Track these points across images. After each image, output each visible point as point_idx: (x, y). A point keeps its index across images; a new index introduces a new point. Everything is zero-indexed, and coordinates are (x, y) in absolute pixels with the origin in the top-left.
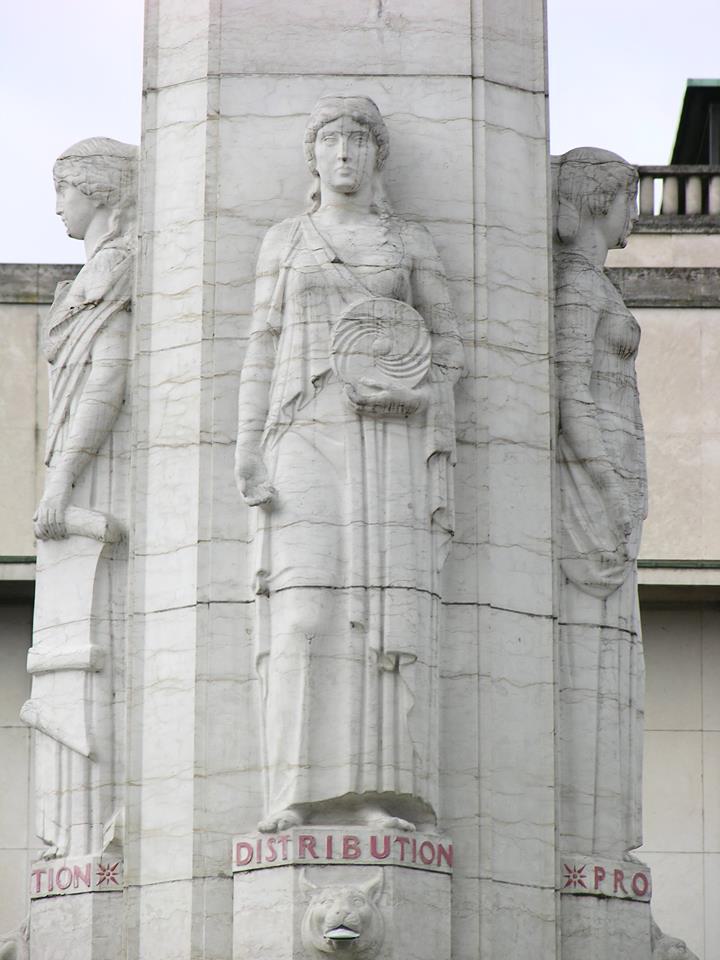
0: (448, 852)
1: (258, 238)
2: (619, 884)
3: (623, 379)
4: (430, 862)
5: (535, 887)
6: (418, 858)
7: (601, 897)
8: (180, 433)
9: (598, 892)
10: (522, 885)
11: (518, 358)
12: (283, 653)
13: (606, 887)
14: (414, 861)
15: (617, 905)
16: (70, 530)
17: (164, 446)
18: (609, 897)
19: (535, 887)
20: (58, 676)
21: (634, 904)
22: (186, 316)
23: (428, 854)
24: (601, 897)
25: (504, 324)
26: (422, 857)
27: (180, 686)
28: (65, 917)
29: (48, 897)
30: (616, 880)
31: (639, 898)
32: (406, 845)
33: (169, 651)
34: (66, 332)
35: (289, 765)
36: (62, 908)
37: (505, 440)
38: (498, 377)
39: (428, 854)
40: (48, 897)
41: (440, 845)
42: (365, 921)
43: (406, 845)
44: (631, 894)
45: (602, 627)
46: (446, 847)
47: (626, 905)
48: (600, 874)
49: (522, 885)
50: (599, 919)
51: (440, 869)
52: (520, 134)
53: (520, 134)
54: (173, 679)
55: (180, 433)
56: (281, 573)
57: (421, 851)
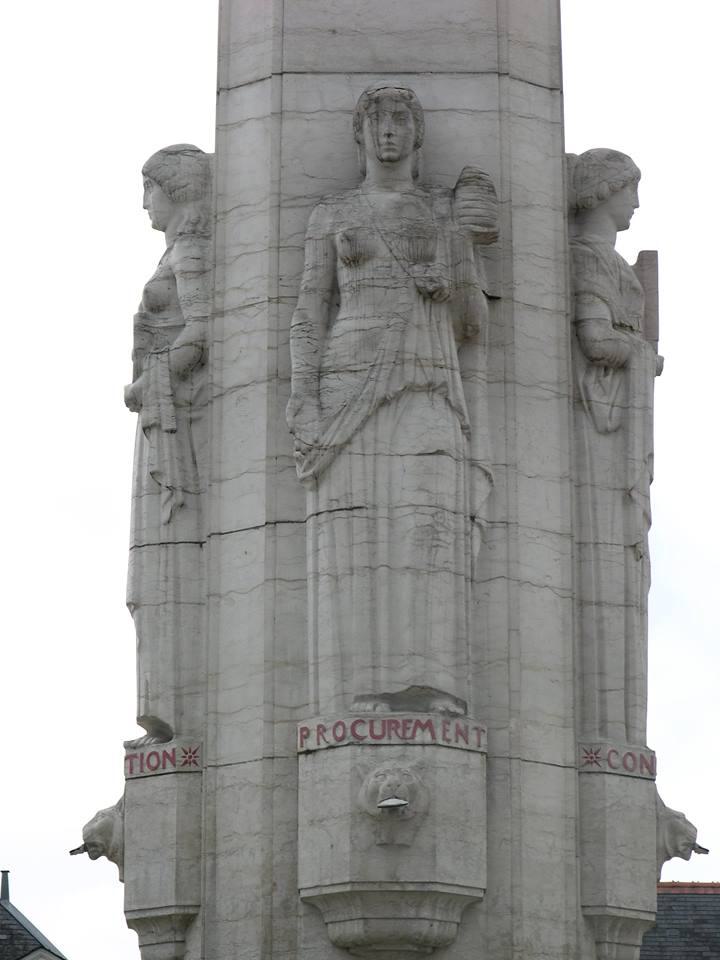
0: (171, 755)
1: (301, 509)
2: (321, 737)
3: (354, 285)
4: (156, 768)
5: (256, 760)
6: (146, 768)
7: (308, 752)
9: (304, 749)
10: (244, 762)
11: (251, 311)
13: (311, 744)
14: (142, 771)
15: (322, 755)
18: (315, 751)
19: (256, 760)
21: (337, 750)
23: (629, 761)
24: (308, 752)
25: (238, 288)
26: (149, 766)
30: (319, 734)
31: (340, 744)
37: (237, 387)
38: (233, 335)
39: (629, 761)
41: (165, 752)
42: (413, 792)
44: (333, 742)
45: (317, 514)
46: (169, 752)
47: (330, 753)
48: (305, 733)
49: (244, 762)
50: (307, 772)
51: (166, 771)
52: (258, 119)
53: (258, 119)
57: (635, 764)
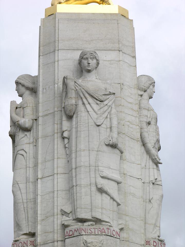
8: (132, 135)
12: (158, 199)
14: (117, 236)
16: (117, 147)
17: (129, 137)
20: (109, 181)
22: (132, 109)
27: (136, 196)
28: (114, 243)
29: (110, 236)
32: (109, 230)
33: (133, 187)
34: (108, 97)
35: (156, 226)
36: (113, 240)
40: (110, 236)
43: (109, 230)
54: (134, 194)
55: (132, 135)
56: (159, 181)
